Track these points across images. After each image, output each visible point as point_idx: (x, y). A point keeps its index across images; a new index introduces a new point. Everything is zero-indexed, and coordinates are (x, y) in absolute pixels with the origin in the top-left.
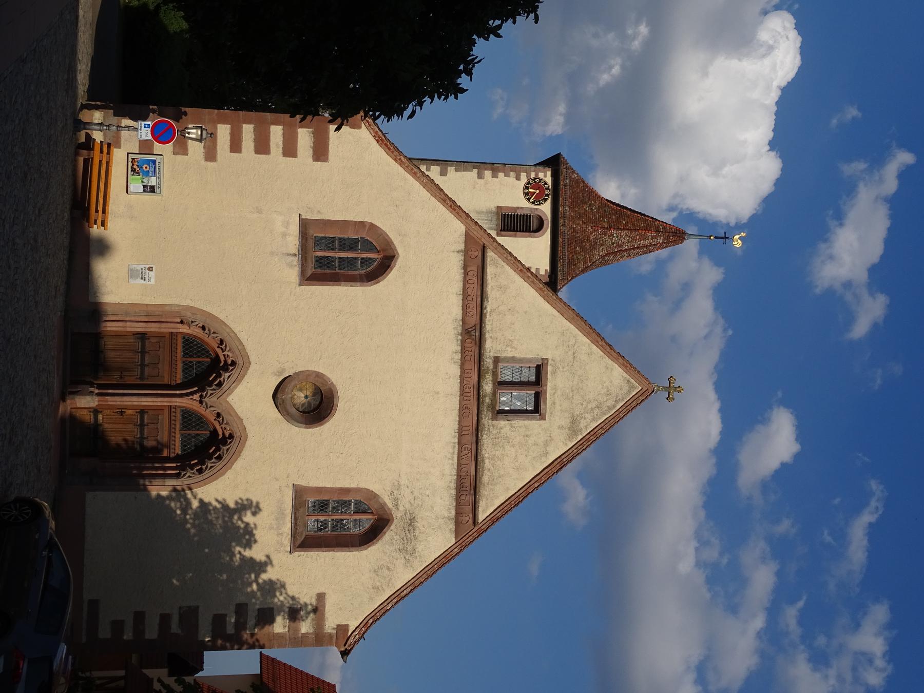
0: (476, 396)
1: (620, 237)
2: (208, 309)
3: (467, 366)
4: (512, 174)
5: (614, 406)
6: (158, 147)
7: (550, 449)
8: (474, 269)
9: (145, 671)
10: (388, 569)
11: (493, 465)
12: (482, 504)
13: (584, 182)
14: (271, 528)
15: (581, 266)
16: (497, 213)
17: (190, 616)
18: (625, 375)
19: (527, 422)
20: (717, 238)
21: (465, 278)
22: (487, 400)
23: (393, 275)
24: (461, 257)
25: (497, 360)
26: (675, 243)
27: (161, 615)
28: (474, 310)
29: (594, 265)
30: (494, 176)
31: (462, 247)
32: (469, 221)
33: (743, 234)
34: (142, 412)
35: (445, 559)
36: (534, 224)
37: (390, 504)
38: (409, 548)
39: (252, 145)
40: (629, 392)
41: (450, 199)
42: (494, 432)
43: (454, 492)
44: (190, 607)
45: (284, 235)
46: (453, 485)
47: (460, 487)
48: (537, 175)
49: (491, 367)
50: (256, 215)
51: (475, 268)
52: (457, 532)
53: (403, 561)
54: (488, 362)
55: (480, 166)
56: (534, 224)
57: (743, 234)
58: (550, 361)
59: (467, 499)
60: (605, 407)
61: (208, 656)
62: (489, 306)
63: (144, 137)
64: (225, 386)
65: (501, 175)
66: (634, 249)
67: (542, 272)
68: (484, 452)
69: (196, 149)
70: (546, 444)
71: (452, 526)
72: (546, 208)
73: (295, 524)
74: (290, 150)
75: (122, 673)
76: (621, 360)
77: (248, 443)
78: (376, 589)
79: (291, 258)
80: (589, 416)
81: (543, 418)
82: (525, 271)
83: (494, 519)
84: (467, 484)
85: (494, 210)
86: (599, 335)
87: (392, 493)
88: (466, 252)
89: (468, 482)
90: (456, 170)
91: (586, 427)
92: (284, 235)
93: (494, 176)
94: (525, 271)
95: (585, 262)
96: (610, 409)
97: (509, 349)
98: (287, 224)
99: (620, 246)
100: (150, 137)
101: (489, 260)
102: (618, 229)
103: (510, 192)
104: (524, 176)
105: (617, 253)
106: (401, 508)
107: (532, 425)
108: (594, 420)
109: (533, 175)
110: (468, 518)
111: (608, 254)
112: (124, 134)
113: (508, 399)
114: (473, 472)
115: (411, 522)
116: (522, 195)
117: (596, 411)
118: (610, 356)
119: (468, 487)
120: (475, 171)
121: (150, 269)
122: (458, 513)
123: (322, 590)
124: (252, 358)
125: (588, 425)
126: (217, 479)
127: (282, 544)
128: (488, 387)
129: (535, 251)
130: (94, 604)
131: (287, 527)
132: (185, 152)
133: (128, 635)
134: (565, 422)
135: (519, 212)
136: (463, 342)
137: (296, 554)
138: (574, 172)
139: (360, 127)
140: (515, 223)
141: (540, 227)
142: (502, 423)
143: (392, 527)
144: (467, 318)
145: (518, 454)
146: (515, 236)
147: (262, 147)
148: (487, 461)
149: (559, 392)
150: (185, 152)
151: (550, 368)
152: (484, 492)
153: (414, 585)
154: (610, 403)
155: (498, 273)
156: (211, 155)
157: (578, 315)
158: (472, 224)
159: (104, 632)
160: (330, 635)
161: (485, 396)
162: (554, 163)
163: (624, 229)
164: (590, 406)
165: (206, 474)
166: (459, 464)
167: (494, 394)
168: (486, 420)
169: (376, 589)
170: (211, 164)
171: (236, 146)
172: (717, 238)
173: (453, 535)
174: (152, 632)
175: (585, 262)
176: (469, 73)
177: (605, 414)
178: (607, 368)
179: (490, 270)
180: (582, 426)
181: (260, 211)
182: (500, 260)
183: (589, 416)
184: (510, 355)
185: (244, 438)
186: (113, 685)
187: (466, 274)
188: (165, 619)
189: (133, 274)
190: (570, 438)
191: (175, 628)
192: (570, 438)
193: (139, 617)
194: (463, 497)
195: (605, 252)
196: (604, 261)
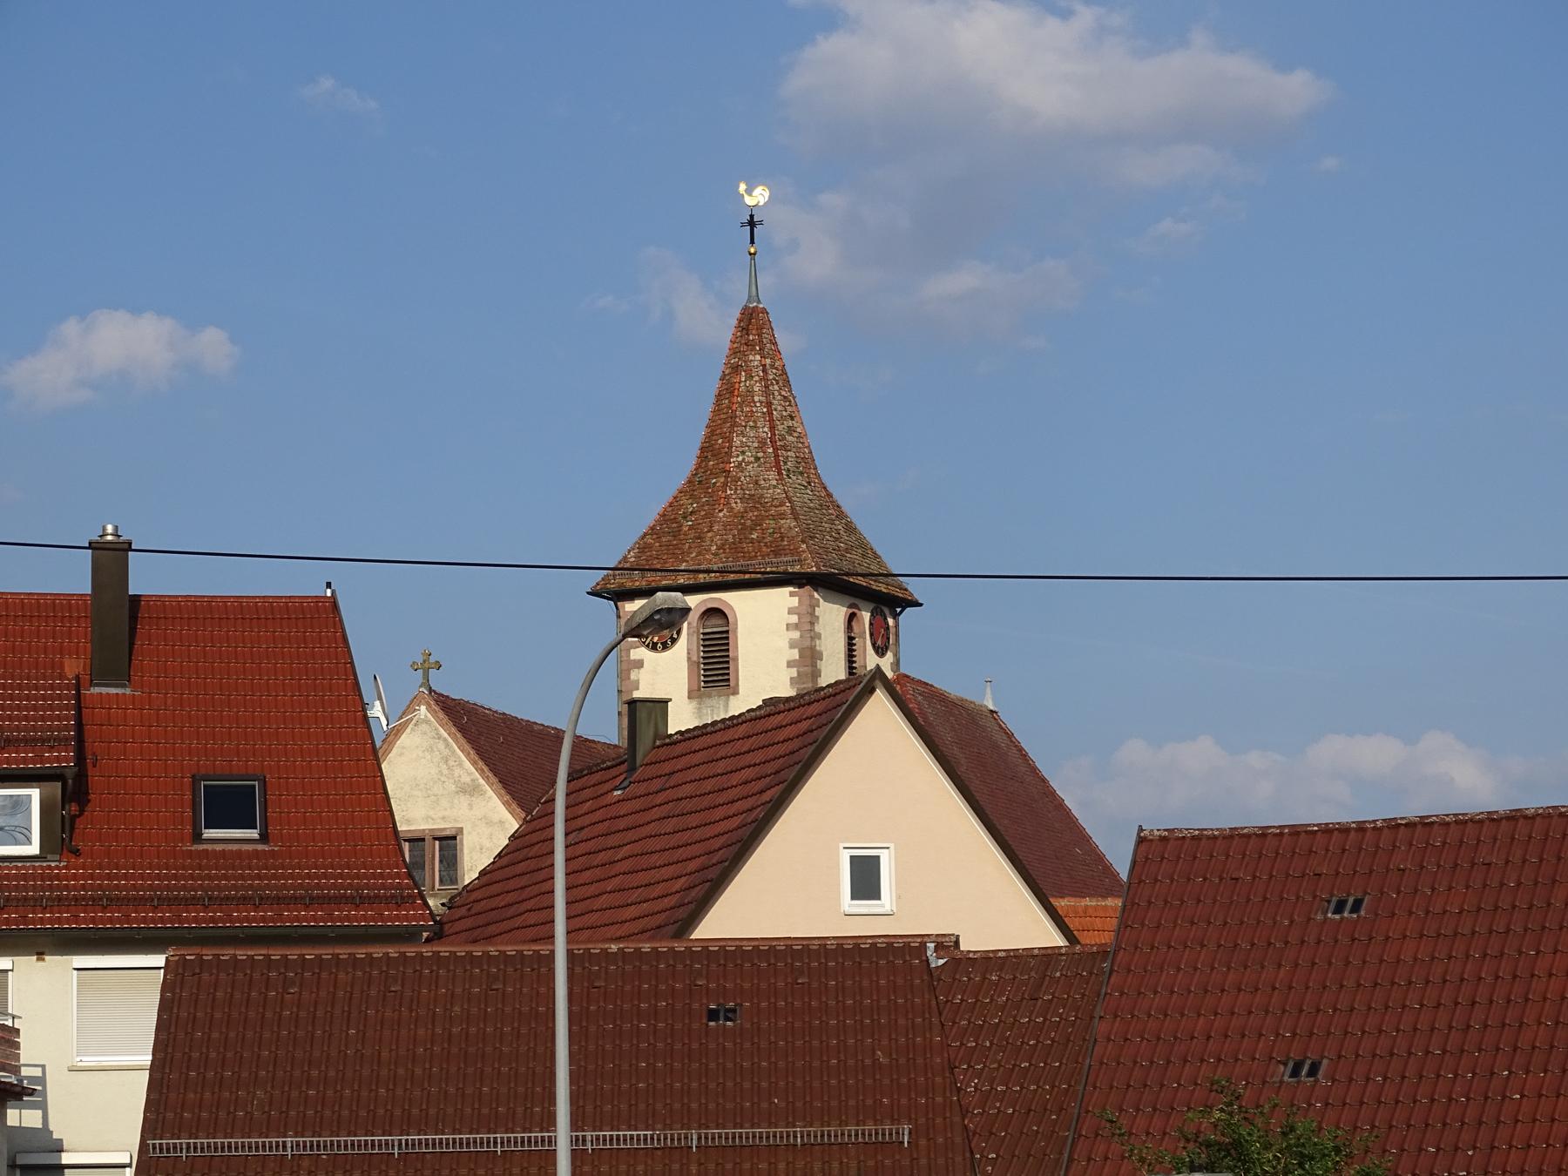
4: (633, 676)
7: (496, 818)
13: (645, 534)
16: (700, 697)
19: (466, 851)
20: (752, 242)
33: (742, 187)
36: (714, 625)
40: (427, 721)
56: (714, 625)
57: (742, 187)
60: (446, 752)
67: (795, 601)
70: (489, 823)
80: (457, 772)
85: (694, 704)
91: (470, 774)
96: (447, 745)
99: (762, 443)
108: (461, 765)
117: (451, 763)
134: (464, 800)
141: (715, 613)
146: (736, 659)
149: (431, 813)
154: (441, 745)
163: (731, 441)
164: (446, 772)
172: (752, 242)
175: (782, 516)
178: (401, 754)
183: (457, 772)
190: (483, 793)
195: (773, 475)
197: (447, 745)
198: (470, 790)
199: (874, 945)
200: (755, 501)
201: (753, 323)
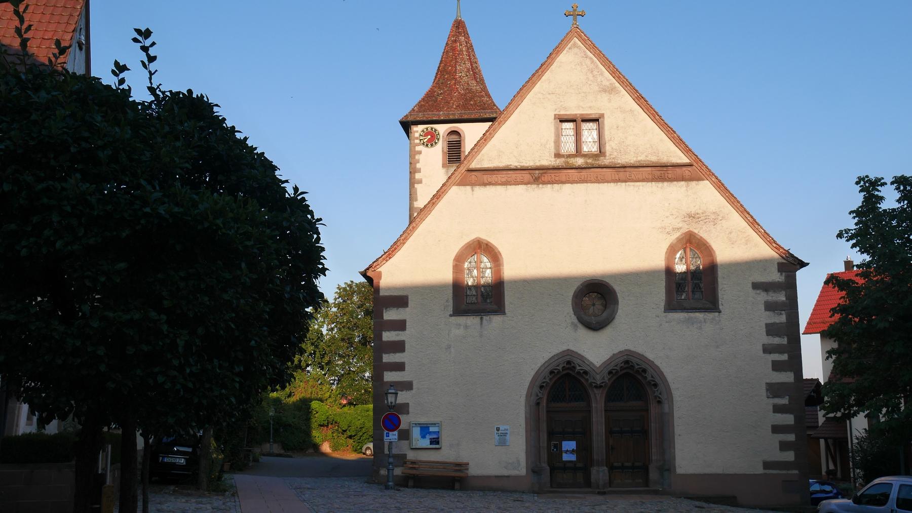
0: (588, 170)
1: (462, 70)
2: (527, 385)
3: (564, 179)
4: (417, 157)
5: (591, 58)
6: (403, 426)
8: (486, 178)
9: (820, 424)
10: (730, 233)
11: (642, 153)
12: (679, 161)
14: (700, 328)
15: (486, 99)
17: (774, 390)
18: (565, 52)
21: (493, 184)
22: (590, 161)
23: (484, 237)
24: (477, 188)
25: (558, 155)
26: (464, 27)
27: (774, 412)
28: (518, 176)
29: (484, 89)
30: (419, 171)
31: (469, 188)
32: (448, 184)
34: (610, 432)
35: (721, 187)
36: (454, 138)
37: (677, 235)
38: (713, 217)
39: (398, 355)
40: (578, 47)
41: (432, 199)
42: (615, 154)
43: (666, 184)
44: (767, 390)
45: (466, 327)
46: (660, 184)
47: (661, 179)
48: (417, 138)
49: (563, 159)
50: (452, 350)
51: (485, 177)
52: (699, 179)
53: (723, 221)
54: (559, 162)
55: (413, 182)
56: (454, 138)
58: (557, 113)
59: (671, 173)
60: (592, 66)
61: (807, 374)
62: (514, 163)
63: (396, 437)
64: (587, 368)
65: (418, 166)
66: (470, 59)
68: (632, 162)
69: (403, 397)
71: (694, 183)
72: (442, 129)
73: (696, 309)
74: (401, 325)
75: (822, 442)
76: (554, 56)
77: (632, 349)
78: (747, 241)
79: (484, 321)
81: (602, 115)
82: (485, 138)
83: (687, 150)
84: (659, 173)
86: (533, 75)
87: (668, 233)
88: (473, 185)
89: (657, 172)
90: (416, 200)
91: (608, 80)
92: (466, 327)
93: (419, 171)
94: (485, 138)
95: (483, 96)
96: (593, 62)
97: (548, 146)
98: (458, 326)
99: (468, 70)
100: (396, 433)
101: (479, 166)
102: (455, 72)
103: (432, 160)
104: (418, 148)
105: (475, 73)
106: (680, 225)
107: (607, 122)
108: (602, 74)
109: (417, 141)
110: (686, 171)
111: (475, 79)
112: (395, 451)
113: (589, 142)
114: (649, 169)
115: (691, 216)
116: (433, 149)
117: (595, 73)
118: (551, 64)
119: (662, 172)
120: (416, 186)
121: (498, 429)
122: (683, 179)
123: (750, 285)
124: (565, 348)
125: (607, 78)
126: (662, 373)
127: (713, 319)
128: (580, 161)
129: (471, 132)
130: (767, 465)
131: (699, 316)
132: (406, 406)
133: (791, 437)
134: (605, 97)
135: (446, 150)
136: (544, 183)
137: (721, 307)
138: (413, 110)
139: (380, 273)
140: (454, 153)
142: (608, 149)
143: (696, 231)
144: (526, 181)
145: (635, 135)
147: (399, 347)
148: (639, 158)
150: (406, 406)
151: (562, 113)
152: (665, 159)
153: (743, 211)
154: (588, 62)
155: (487, 158)
156: (408, 386)
157: (518, 93)
158: (450, 181)
159: (790, 456)
160: (787, 277)
161: (587, 163)
162: (406, 126)
165: (658, 380)
166: (643, 180)
167: (585, 156)
168: (606, 161)
169: (747, 241)
170: (415, 386)
171: (400, 367)
173: (701, 182)
174: (788, 419)
175: (483, 96)
176: (256, 148)
177: (597, 66)
179: (486, 165)
180: (608, 83)
181: (449, 347)
182: (479, 157)
184: (553, 144)
185: (629, 353)
186: (832, 448)
187: (490, 184)
188: (777, 409)
189: (502, 443)
190: (618, 92)
191: (785, 401)
192: (618, 92)
193: (776, 429)
194: (670, 176)
195: (474, 82)
196: (481, 82)
197: (593, 62)
198: (610, 90)
199: (840, 309)
200: (469, 90)
201: (459, 26)
